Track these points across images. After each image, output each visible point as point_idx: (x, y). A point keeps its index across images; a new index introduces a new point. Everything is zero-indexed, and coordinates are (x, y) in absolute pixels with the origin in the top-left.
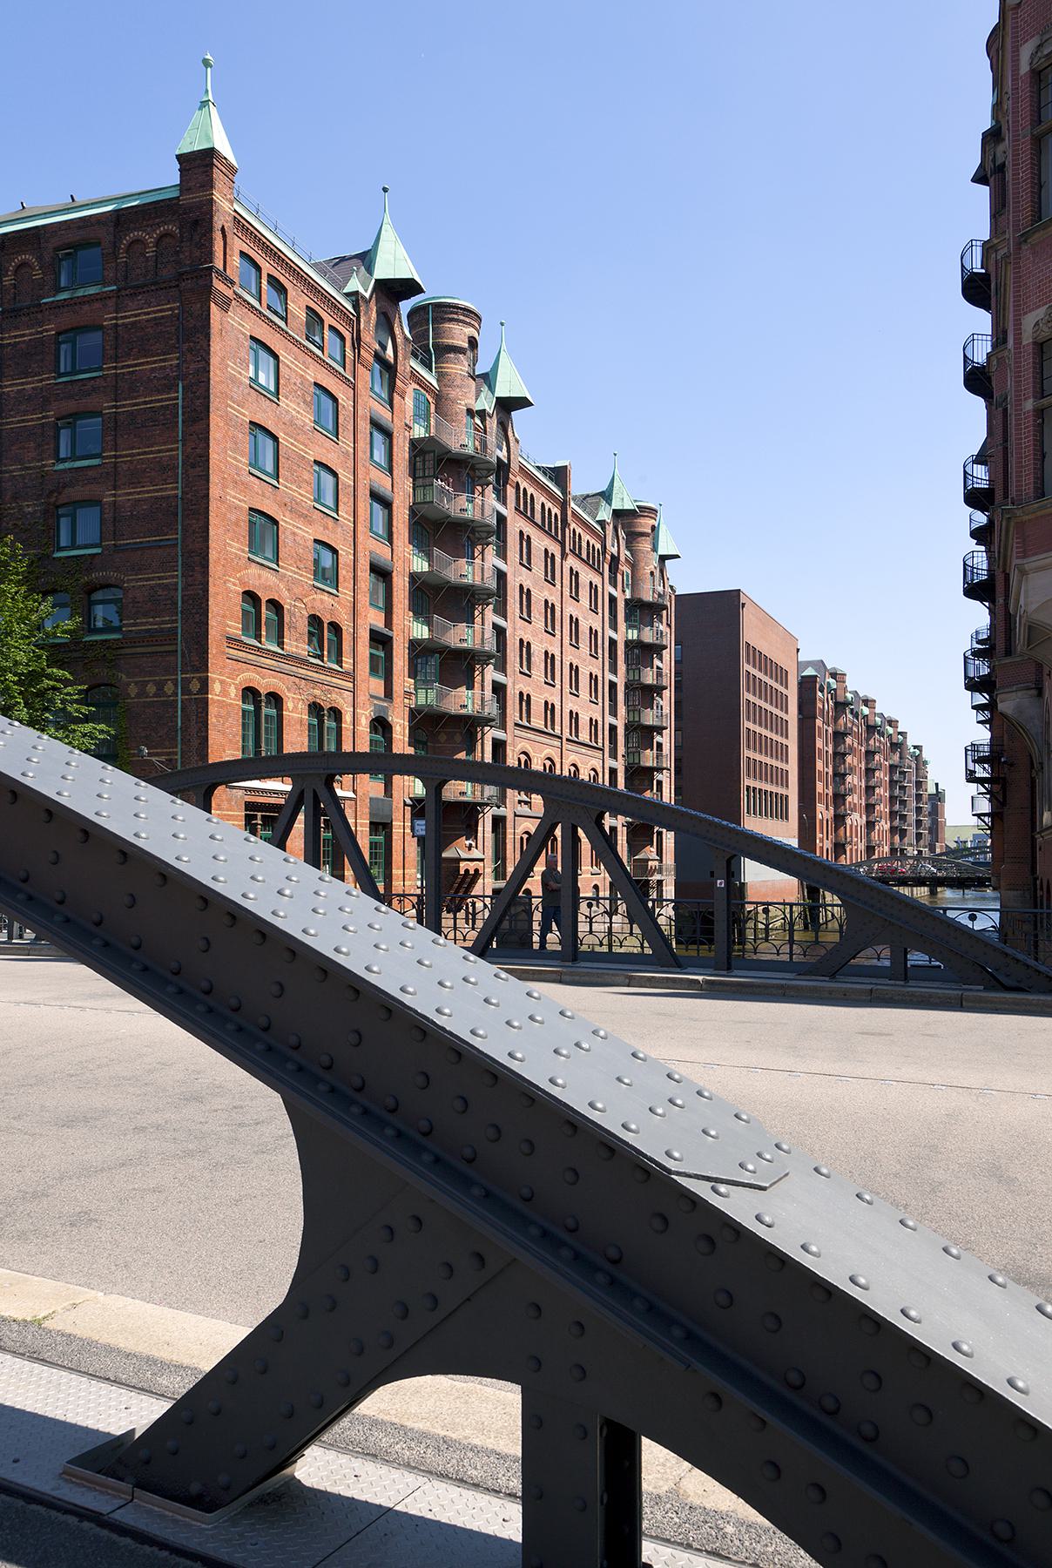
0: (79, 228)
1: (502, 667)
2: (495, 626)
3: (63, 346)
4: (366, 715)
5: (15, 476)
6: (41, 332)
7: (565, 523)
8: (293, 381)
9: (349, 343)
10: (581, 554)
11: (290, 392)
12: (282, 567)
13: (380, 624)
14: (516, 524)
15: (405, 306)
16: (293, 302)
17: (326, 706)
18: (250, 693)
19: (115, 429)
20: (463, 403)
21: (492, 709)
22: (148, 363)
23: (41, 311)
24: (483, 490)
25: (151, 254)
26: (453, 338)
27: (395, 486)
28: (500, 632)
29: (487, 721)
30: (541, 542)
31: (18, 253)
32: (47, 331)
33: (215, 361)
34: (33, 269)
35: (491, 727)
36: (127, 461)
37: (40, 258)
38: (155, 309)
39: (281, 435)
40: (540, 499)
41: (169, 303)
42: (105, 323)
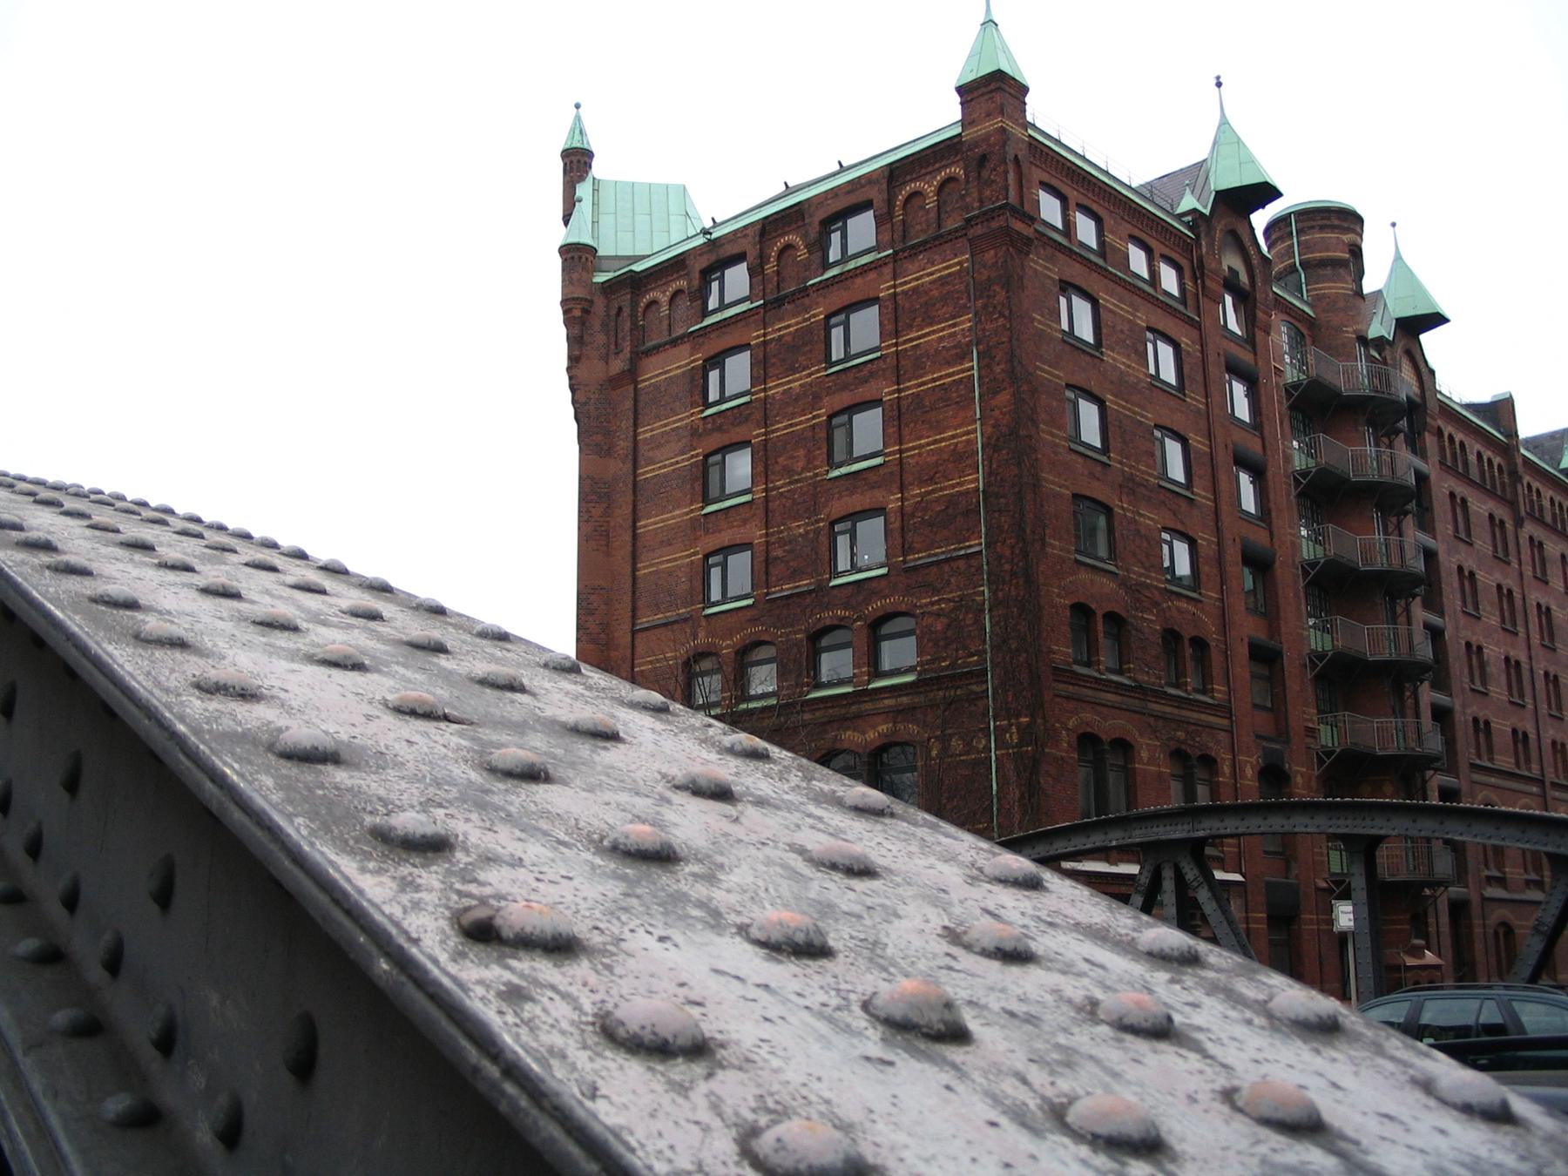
0: (848, 193)
1: (1441, 684)
2: (1427, 626)
3: (834, 332)
4: (1252, 763)
5: (782, 493)
6: (809, 319)
7: (1515, 477)
8: (1119, 328)
9: (1187, 273)
10: (1542, 516)
13: (1261, 635)
14: (1443, 486)
15: (1260, 219)
16: (1112, 232)
17: (1187, 633)
18: (1088, 741)
19: (899, 417)
20: (1350, 329)
21: (1434, 743)
22: (934, 332)
23: (808, 295)
24: (1390, 442)
25: (931, 205)
28: (1436, 634)
29: (1426, 762)
30: (1480, 506)
31: (782, 235)
32: (814, 316)
34: (798, 250)
36: (915, 455)
37: (804, 237)
38: (941, 266)
39: (1116, 504)
40: (1473, 447)
42: (881, 295)
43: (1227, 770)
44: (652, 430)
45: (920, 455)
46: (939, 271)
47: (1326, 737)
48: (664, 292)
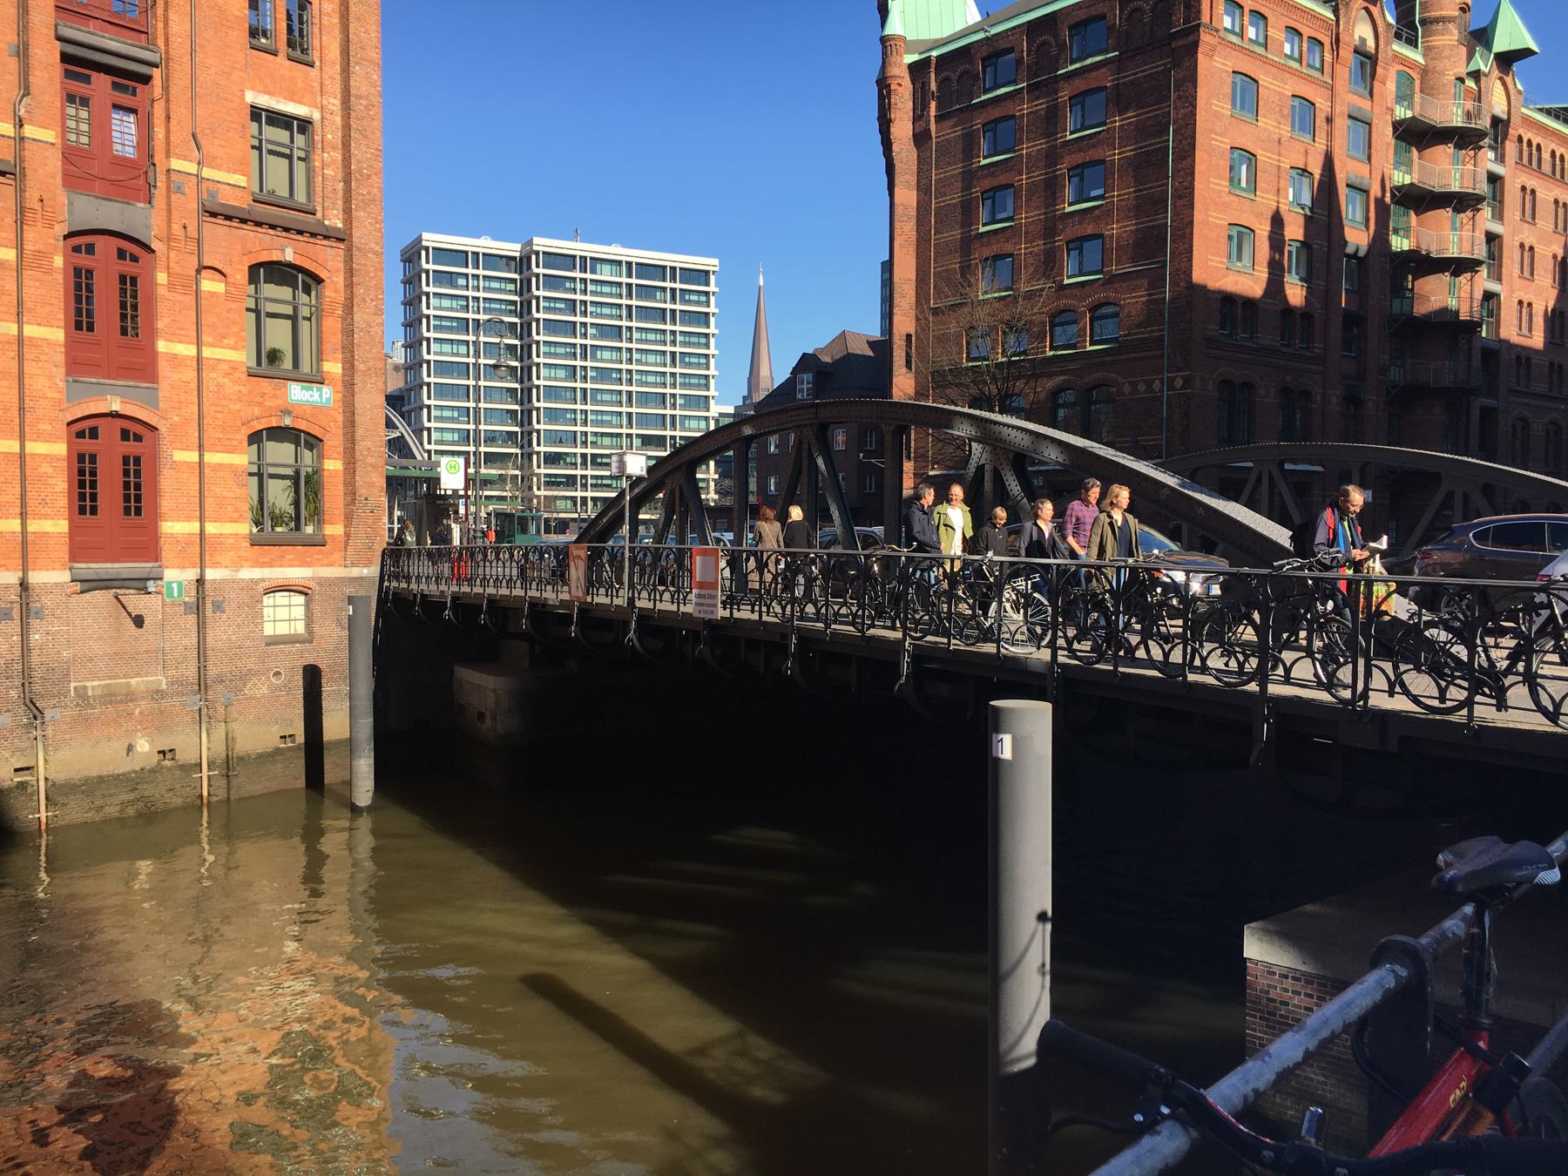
11: (1268, 111)
12: (1258, 271)
26: (1441, 9)
27: (1373, 172)
31: (1041, 35)
33: (1200, 103)
35: (1478, 396)
39: (1258, 152)
41: (1162, 59)
43: (1319, 399)
44: (945, 172)
45: (1128, 199)
46: (1150, 69)
47: (1395, 374)
48: (954, 72)
